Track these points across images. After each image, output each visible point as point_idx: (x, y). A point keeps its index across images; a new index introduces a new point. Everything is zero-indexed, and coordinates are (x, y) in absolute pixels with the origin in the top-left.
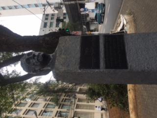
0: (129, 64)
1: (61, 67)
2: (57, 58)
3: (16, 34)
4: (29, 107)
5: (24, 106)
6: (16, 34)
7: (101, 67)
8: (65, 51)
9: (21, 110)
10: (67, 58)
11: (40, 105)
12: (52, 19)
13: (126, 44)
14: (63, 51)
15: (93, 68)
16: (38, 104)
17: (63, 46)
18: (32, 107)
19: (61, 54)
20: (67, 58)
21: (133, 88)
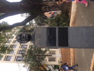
0: (69, 44)
1: (38, 45)
2: (36, 40)
3: (14, 3)
4: (13, 43)
5: (12, 39)
6: (14, 3)
7: (56, 46)
8: (39, 36)
9: (11, 41)
10: (40, 40)
11: (17, 46)
12: (67, 6)
13: (69, 33)
14: (38, 36)
15: (53, 46)
16: (16, 45)
17: (38, 33)
18: (14, 43)
19: (37, 38)
20: (40, 40)
21: (22, 29)
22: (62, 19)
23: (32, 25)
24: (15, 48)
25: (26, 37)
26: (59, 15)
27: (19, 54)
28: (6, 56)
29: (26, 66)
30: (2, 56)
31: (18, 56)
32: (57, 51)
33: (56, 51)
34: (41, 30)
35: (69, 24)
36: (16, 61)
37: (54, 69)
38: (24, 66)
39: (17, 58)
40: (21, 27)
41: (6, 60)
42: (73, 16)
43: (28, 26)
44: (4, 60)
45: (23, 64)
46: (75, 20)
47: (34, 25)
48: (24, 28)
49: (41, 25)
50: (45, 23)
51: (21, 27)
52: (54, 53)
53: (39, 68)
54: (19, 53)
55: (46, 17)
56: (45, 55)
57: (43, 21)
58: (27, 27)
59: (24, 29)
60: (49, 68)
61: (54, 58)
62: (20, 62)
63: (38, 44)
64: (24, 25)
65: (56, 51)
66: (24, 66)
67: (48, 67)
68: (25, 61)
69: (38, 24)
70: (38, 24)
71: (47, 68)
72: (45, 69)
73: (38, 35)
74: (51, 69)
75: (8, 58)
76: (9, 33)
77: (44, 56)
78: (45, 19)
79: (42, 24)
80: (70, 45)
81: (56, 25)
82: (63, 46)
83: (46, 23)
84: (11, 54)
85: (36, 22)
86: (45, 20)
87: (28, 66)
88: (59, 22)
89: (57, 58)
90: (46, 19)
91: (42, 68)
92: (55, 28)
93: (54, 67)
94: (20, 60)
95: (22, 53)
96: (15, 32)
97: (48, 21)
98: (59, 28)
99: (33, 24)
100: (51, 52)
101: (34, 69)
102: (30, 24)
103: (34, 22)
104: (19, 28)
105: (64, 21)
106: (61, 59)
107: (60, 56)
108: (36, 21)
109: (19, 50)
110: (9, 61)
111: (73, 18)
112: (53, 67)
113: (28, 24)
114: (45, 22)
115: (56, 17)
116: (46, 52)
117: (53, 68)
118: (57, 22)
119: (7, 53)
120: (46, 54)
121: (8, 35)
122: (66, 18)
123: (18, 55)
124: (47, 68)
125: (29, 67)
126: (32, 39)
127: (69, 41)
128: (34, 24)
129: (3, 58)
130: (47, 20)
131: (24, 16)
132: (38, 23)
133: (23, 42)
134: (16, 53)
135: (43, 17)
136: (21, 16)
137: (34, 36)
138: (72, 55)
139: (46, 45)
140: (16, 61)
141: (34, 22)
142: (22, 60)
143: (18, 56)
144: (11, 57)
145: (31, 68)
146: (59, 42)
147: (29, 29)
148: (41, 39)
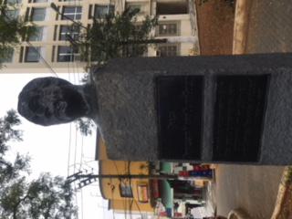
0: (263, 152)
7: (203, 158)
13: (269, 104)
17: (114, 106)
20: (127, 134)
24: (42, 19)
27: (60, 39)
28: (22, 48)
30: (11, 51)
32: (183, 23)
33: (179, 21)
34: (127, 90)
39: (59, 52)
41: (26, 61)
44: (21, 61)
52: (173, 29)
54: (60, 35)
56: (144, 39)
61: (175, 25)
63: (120, 150)
65: (179, 21)
73: (112, 111)
75: (29, 54)
77: (144, 42)
84: (37, 42)
89: (182, 45)
94: (67, 59)
95: (69, 38)
100: (165, 27)
106: (195, 50)
107: (195, 38)
109: (56, 26)
110: (37, 62)
116: (147, 33)
119: (20, 40)
120: (149, 39)
123: (58, 43)
129: (16, 57)
134: (50, 60)
138: (238, 36)
140: (58, 60)
142: (77, 59)
144: (44, 9)
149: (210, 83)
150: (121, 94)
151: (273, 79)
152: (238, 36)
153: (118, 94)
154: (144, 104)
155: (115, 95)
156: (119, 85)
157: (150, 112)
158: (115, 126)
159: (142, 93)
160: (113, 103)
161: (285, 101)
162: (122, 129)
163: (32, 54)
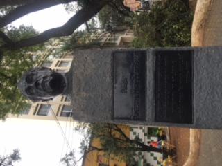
0: (196, 115)
4: (56, 66)
8: (86, 84)
13: (195, 72)
14: (83, 84)
17: (83, 73)
22: (170, 14)
23: (94, 32)
25: (43, 83)
26: (163, 4)
29: (81, 128)
30: (29, 106)
31: (64, 106)
34: (93, 61)
35: (190, 28)
36: (61, 115)
37: (146, 137)
38: (76, 129)
39: (63, 109)
40: (67, 38)
41: (38, 114)
42: (203, 4)
43: (81, 34)
44: (34, 114)
45: (76, 124)
46: (209, 15)
47: (99, 31)
48: (74, 41)
49: (116, 31)
50: (124, 27)
51: (67, 38)
53: (112, 134)
55: (128, 9)
57: (120, 21)
58: (81, 37)
59: (75, 41)
60: (135, 133)
62: (69, 118)
64: (70, 34)
66: (76, 129)
67: (132, 130)
68: (76, 117)
69: (109, 29)
70: (107, 30)
71: (131, 133)
72: (123, 134)
73: (81, 78)
74: (140, 135)
76: (39, 53)
78: (125, 15)
79: (118, 28)
80: (198, 119)
81: (154, 30)
82: (174, 122)
83: (127, 26)
85: (104, 24)
86: (127, 19)
87: (86, 129)
88: (161, 21)
90: (128, 15)
91: (118, 135)
92: (143, 54)
93: (146, 131)
94: (68, 115)
96: (54, 51)
97: (134, 21)
98: (157, 53)
99: (95, 28)
101: (100, 136)
102: (88, 29)
103: (96, 22)
104: (62, 41)
105: (176, 21)
108: (104, 19)
111: (204, 11)
112: (144, 131)
113: (82, 28)
114: (127, 23)
115: (154, 10)
117: (145, 135)
118: (157, 22)
121: (38, 57)
122: (182, 12)
124: (131, 133)
125: (88, 132)
126: (65, 89)
127: (195, 103)
128: (99, 28)
129: (32, 110)
130: (132, 18)
131: (72, 10)
132: (108, 26)
133: (39, 97)
135: (120, 12)
136: (67, 9)
137: (70, 82)
138: (192, 139)
139: (109, 116)
141: (96, 22)
143: (64, 106)
145: (92, 133)
146: (156, 107)
147: (87, 42)
148: (92, 96)
149: (150, 54)
150: (89, 65)
151: (195, 53)
152: (192, 139)
153: (87, 64)
154: (104, 73)
155: (84, 65)
156: (88, 58)
157: (108, 78)
158: (82, 90)
159: (103, 63)
160: (82, 70)
161: (207, 70)
162: (86, 92)
163: (43, 110)
